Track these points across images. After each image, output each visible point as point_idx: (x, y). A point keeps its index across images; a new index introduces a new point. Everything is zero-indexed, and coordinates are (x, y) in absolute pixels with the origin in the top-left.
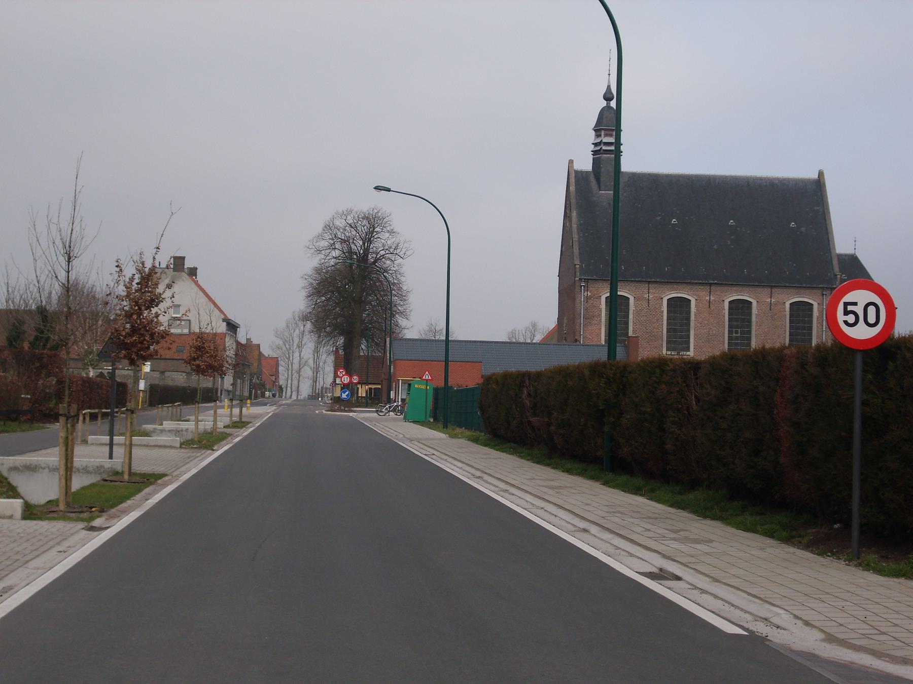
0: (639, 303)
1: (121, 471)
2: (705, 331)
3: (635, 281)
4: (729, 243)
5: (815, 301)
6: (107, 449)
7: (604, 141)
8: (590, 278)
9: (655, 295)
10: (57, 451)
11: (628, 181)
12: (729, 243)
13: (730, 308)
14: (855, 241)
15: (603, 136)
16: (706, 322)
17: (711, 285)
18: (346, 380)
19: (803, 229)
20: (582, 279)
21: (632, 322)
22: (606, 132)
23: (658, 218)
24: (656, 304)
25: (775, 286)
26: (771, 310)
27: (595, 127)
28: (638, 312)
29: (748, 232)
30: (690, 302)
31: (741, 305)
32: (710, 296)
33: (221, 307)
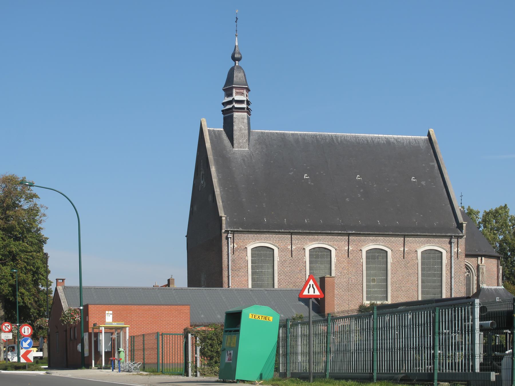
0: (283, 254)
1: (378, 381)
2: (345, 280)
3: (279, 232)
4: (359, 196)
5: (443, 249)
6: (146, 347)
7: (236, 99)
8: (236, 230)
9: (298, 246)
10: (482, 259)
11: (258, 139)
12: (359, 196)
13: (367, 258)
14: (461, 196)
15: (234, 94)
16: (345, 271)
17: (349, 235)
18: (26, 331)
19: (423, 183)
20: (228, 231)
21: (277, 273)
22: (238, 91)
23: (291, 174)
24: (299, 255)
25: (408, 235)
26: (404, 258)
27: (225, 86)
28: (282, 263)
29: (375, 186)
30: (209, 285)
31: (377, 254)
32: (348, 246)
33: (246, 77)
